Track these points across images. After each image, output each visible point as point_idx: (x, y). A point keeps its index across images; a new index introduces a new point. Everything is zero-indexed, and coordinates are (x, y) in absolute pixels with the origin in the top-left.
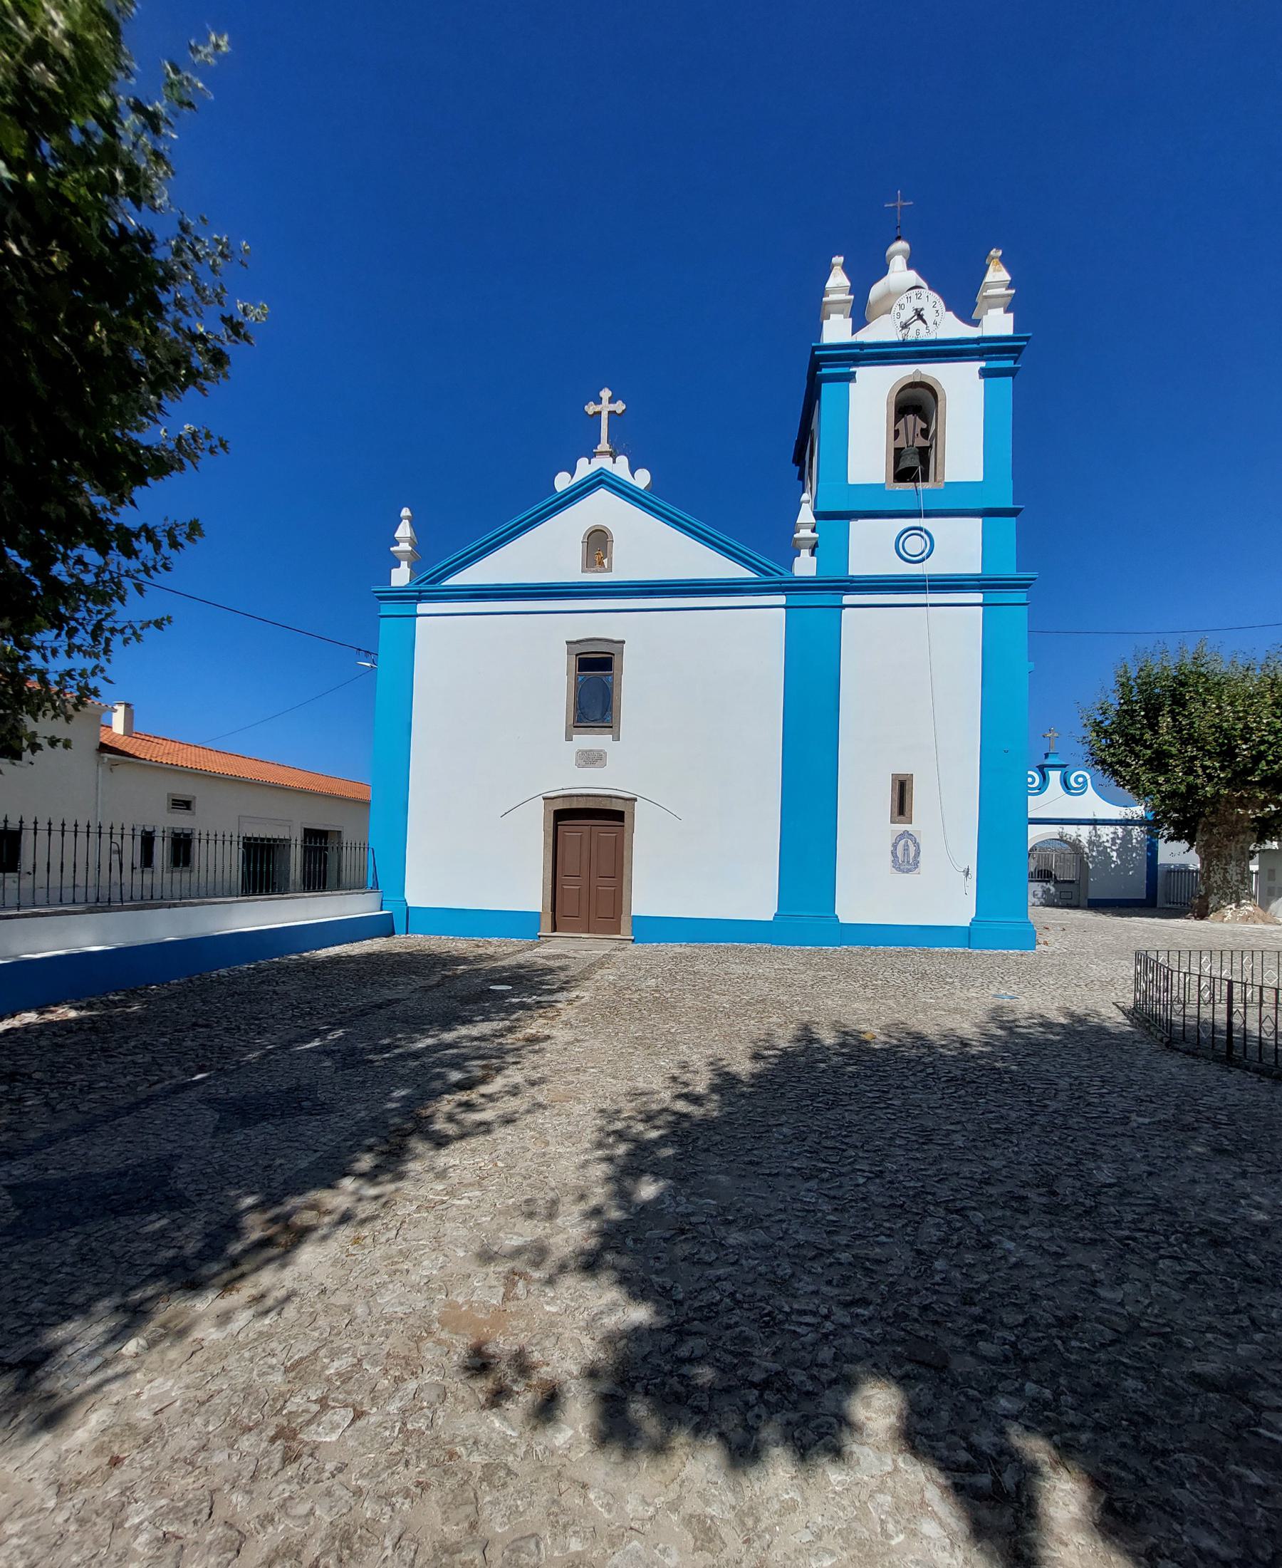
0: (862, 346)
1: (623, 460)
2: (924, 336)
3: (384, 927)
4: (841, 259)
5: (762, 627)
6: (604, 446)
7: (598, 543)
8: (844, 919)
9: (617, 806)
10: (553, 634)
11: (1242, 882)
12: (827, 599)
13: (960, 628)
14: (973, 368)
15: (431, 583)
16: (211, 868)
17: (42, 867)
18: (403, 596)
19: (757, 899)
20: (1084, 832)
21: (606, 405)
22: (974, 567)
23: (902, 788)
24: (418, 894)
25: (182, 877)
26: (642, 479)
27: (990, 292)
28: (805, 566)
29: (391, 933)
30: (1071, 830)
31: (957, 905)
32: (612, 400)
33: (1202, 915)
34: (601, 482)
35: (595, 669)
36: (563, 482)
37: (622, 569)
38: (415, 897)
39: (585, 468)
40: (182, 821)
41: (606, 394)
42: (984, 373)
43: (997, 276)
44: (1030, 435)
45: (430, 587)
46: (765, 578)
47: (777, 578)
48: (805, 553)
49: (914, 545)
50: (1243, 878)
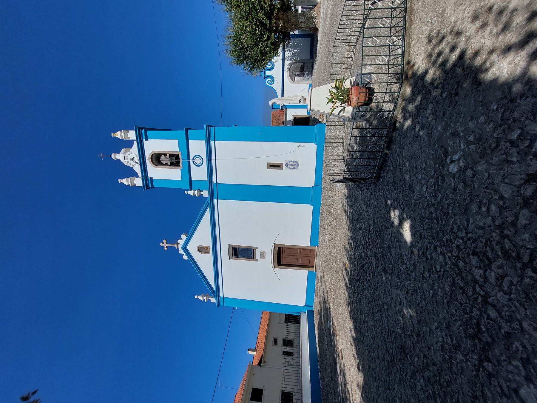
0: (142, 176)
1: (179, 242)
2: (138, 158)
3: (311, 313)
4: (119, 180)
5: (223, 206)
6: (175, 246)
7: (202, 250)
9: (277, 249)
10: (229, 265)
11: (305, 16)
12: (215, 187)
13: (223, 148)
14: (145, 143)
16: (293, 372)
17: (292, 387)
19: (307, 210)
20: (287, 62)
22: (204, 142)
23: (272, 166)
24: (302, 302)
25: (295, 344)
26: (184, 237)
27: (123, 137)
28: (205, 194)
29: (312, 312)
30: (286, 67)
31: (311, 149)
32: (163, 243)
33: (317, 30)
35: (237, 252)
36: (185, 257)
37: (209, 243)
38: (302, 303)
39: (181, 252)
40: (280, 342)
41: (161, 245)
43: (119, 135)
44: (163, 127)
45: (216, 293)
46: (210, 205)
47: (209, 202)
48: (202, 193)
49: (198, 161)
50: (304, 16)
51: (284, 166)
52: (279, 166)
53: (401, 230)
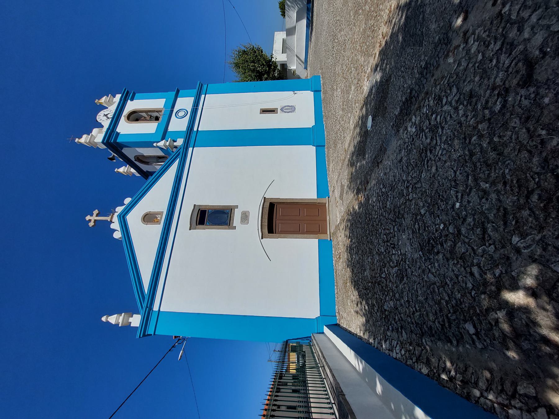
2: (112, 114)
6: (108, 219)
7: (149, 218)
8: (313, 124)
9: (267, 205)
12: (193, 136)
15: (144, 301)
16: (301, 399)
18: (146, 321)
21: (92, 218)
23: (264, 111)
28: (180, 142)
34: (124, 217)
35: (205, 217)
36: (117, 235)
37: (163, 207)
39: (116, 225)
41: (91, 224)
42: (132, 99)
45: (146, 303)
47: (181, 150)
49: (181, 114)
51: (279, 110)
52: (274, 111)
53: (532, 317)
